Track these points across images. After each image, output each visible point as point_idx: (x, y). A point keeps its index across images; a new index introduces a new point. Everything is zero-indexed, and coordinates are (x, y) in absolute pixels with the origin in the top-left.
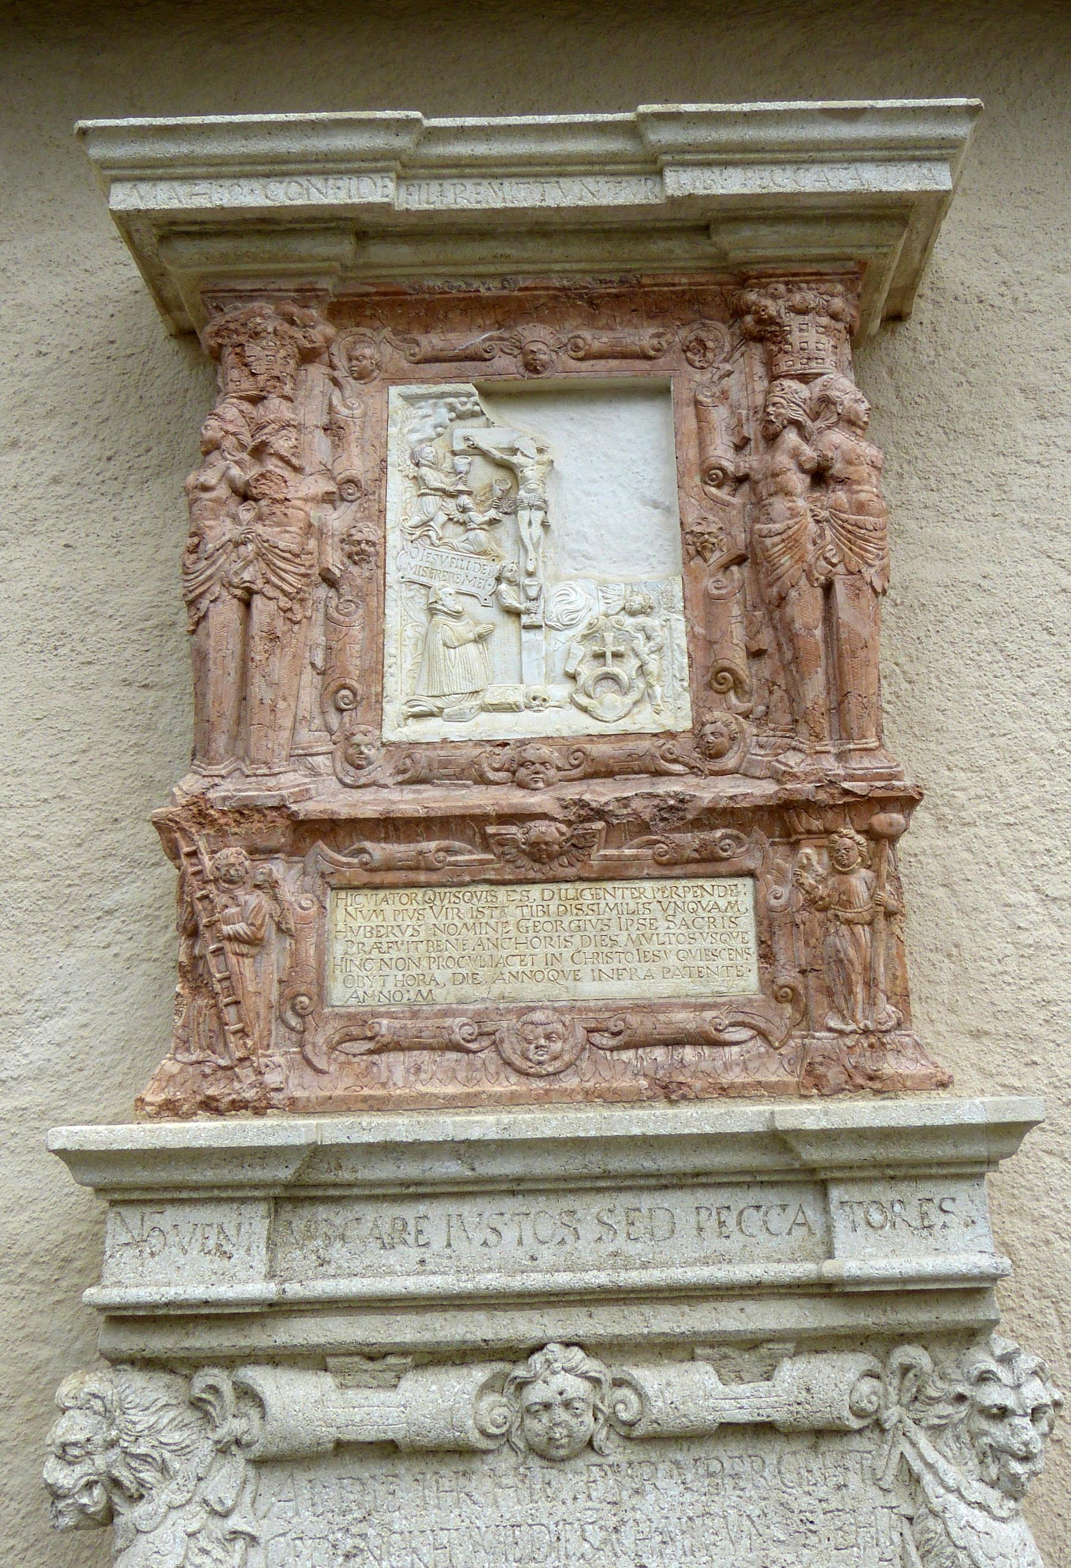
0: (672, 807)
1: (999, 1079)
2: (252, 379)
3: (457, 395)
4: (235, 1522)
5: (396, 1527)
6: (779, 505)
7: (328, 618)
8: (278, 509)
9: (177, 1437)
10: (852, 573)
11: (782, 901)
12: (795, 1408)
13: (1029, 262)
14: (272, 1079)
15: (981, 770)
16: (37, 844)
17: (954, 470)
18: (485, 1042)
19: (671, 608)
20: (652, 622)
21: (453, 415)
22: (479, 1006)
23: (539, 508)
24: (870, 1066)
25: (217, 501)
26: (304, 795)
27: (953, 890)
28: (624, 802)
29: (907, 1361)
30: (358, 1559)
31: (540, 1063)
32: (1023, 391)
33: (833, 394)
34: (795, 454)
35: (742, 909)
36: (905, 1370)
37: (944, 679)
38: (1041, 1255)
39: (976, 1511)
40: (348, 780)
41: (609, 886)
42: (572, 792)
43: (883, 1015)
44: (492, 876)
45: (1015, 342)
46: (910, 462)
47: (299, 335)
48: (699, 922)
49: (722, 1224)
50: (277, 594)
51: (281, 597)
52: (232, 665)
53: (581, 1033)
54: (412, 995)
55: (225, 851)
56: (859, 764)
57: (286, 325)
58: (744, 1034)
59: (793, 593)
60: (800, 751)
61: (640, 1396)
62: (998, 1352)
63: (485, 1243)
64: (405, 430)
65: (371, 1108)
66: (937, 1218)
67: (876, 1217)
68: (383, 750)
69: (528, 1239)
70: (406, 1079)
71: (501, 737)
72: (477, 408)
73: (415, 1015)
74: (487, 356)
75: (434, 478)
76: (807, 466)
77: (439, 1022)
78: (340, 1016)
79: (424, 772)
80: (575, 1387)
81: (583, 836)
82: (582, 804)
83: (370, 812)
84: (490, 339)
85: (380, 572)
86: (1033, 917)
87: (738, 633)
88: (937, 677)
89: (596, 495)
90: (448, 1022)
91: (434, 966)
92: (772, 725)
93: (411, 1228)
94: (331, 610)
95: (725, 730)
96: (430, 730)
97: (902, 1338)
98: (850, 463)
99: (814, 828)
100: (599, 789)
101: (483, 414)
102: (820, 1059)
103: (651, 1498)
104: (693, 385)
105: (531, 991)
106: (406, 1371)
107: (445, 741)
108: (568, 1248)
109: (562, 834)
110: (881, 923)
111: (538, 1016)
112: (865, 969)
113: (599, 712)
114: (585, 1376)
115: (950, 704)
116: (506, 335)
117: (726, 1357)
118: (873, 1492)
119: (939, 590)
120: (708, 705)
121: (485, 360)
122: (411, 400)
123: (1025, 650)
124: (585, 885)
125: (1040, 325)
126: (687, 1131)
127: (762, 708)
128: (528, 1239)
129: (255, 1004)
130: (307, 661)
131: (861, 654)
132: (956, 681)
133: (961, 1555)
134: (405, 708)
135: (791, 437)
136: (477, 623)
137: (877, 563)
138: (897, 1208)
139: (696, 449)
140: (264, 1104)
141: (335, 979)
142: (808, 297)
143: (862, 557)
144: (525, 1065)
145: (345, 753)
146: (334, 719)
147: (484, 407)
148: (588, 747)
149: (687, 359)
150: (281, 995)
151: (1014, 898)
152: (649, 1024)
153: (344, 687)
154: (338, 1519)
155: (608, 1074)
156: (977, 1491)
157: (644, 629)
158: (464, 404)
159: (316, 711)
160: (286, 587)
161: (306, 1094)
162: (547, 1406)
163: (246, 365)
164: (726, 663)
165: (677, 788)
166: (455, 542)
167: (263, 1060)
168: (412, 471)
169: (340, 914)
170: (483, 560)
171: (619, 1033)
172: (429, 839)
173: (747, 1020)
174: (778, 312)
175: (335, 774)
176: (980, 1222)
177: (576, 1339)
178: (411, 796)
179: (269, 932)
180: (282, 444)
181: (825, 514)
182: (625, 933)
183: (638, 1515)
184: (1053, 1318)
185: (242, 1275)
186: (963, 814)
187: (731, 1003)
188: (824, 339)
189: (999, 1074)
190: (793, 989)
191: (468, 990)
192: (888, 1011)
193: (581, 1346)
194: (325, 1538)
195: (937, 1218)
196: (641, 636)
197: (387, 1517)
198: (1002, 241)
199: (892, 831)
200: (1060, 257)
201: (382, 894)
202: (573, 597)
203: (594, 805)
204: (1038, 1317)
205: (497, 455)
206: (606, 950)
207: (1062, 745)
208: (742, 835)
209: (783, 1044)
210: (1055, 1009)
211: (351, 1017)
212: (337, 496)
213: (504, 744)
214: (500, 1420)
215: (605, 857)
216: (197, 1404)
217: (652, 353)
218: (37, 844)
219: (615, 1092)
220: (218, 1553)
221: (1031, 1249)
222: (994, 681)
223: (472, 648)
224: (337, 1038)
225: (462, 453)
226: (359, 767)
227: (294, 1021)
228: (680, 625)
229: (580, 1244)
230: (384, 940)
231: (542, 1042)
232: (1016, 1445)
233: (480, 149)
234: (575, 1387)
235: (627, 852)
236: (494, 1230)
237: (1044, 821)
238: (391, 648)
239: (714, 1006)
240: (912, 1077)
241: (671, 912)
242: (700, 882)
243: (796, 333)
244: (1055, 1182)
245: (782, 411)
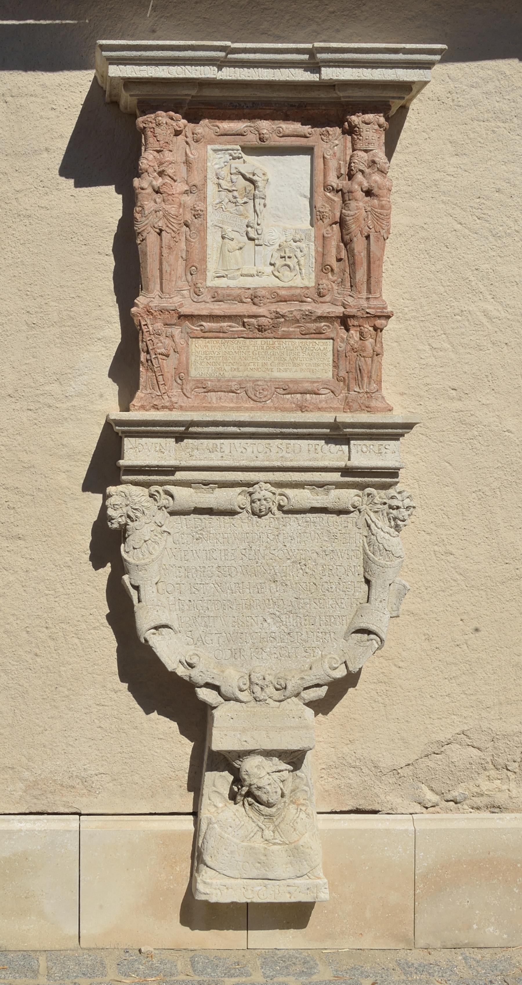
0: (306, 315)
1: (408, 409)
2: (157, 142)
3: (233, 150)
4: (164, 528)
5: (211, 532)
6: (353, 204)
7: (186, 239)
8: (170, 198)
9: (146, 504)
10: (376, 232)
11: (342, 349)
12: (334, 503)
13: (461, 83)
14: (174, 399)
15: (415, 300)
16: (72, 314)
17: (419, 178)
18: (242, 390)
19: (310, 240)
20: (302, 245)
21: (231, 157)
22: (240, 379)
23: (263, 199)
24: (367, 403)
25: (148, 194)
26: (181, 305)
27: (400, 344)
28: (291, 312)
29: (369, 492)
30: (200, 540)
31: (260, 398)
32: (451, 142)
33: (377, 159)
34: (360, 184)
35: (328, 350)
36: (369, 495)
37: (405, 264)
38: (415, 467)
39: (386, 534)
40: (195, 300)
41: (284, 340)
42: (273, 307)
43: (372, 388)
44: (245, 336)
45: (451, 120)
46: (402, 173)
47: (174, 124)
48: (314, 354)
49: (316, 449)
50: (171, 231)
51: (173, 233)
52: (157, 258)
53: (273, 389)
54: (218, 374)
55: (157, 324)
56: (373, 303)
57: (170, 120)
58: (327, 391)
59: (355, 239)
60: (352, 297)
61: (287, 498)
62: (398, 491)
63: (242, 452)
64: (213, 164)
65: (206, 410)
66: (384, 451)
67: (365, 449)
68: (207, 289)
69: (255, 451)
70: (217, 402)
71: (248, 286)
72: (240, 155)
73: (219, 381)
74: (245, 134)
75: (225, 184)
76: (364, 189)
77: (227, 383)
78: (194, 380)
79: (221, 298)
80: (269, 495)
81: (276, 323)
82: (277, 313)
83: (205, 312)
84: (246, 126)
85: (205, 222)
86: (427, 355)
87: (334, 251)
88: (403, 263)
89: (283, 192)
90: (230, 384)
91: (225, 365)
92: (343, 286)
93: (219, 447)
94: (188, 237)
95: (326, 287)
96: (223, 283)
97: (368, 486)
98: (380, 189)
99: (355, 325)
100: (282, 307)
101: (242, 157)
102: (350, 401)
103: (288, 527)
104: (323, 149)
105: (257, 375)
106: (215, 489)
107: (228, 287)
108: (267, 454)
109: (270, 323)
110: (375, 357)
111: (259, 383)
112: (368, 372)
113: (282, 278)
114: (270, 492)
115: (406, 274)
116: (252, 125)
117: (314, 489)
118: (355, 528)
119: (407, 228)
120: (321, 277)
121: (244, 136)
122: (215, 151)
123: (437, 254)
124: (276, 340)
125: (462, 112)
126: (308, 421)
127: (340, 280)
128: (255, 451)
129: (168, 375)
130: (180, 256)
131: (377, 263)
132: (409, 265)
133: (380, 545)
134: (214, 274)
135: (359, 176)
136: (239, 243)
137: (386, 228)
138: (371, 447)
139: (323, 177)
140: (172, 407)
141: (192, 368)
142: (370, 117)
143: (381, 226)
144: (255, 398)
145: (194, 290)
146: (189, 277)
147: (243, 155)
148: (278, 291)
149: (322, 138)
150: (175, 373)
151: (420, 347)
152: (296, 387)
153: (193, 266)
154: (194, 529)
155: (282, 402)
156: (387, 529)
157: (300, 248)
158: (235, 153)
159: (183, 274)
160: (174, 229)
161: (185, 405)
162: (259, 500)
163: (155, 137)
164: (329, 263)
165: (309, 308)
166: (231, 210)
167: (171, 394)
168: (216, 181)
169: (193, 346)
170: (242, 218)
171: (286, 390)
172: (224, 322)
173: (328, 387)
174: (359, 122)
175: (190, 297)
176: (397, 452)
177: (268, 481)
178: (217, 307)
179: (172, 352)
180: (170, 171)
181: (369, 209)
182: (289, 357)
183: (284, 532)
184: (416, 486)
185: (168, 458)
186: (406, 316)
187: (323, 381)
188: (375, 135)
189: (408, 408)
190: (344, 378)
191: (236, 373)
192: (374, 386)
193: (270, 483)
194: (190, 534)
195: (384, 451)
196: (298, 250)
197: (209, 529)
198: (451, 72)
199: (381, 327)
200: (475, 80)
201: (207, 340)
202: (274, 234)
203: (281, 313)
204: (412, 485)
205: (248, 176)
206: (282, 362)
207: (446, 292)
208: (330, 325)
209: (339, 395)
210: (430, 387)
211: (198, 381)
212: (189, 192)
213: (249, 289)
214: (244, 503)
215: (284, 331)
216: (151, 496)
217: (308, 135)
218: (72, 314)
219: (284, 408)
220: (160, 536)
221: (412, 465)
222: (424, 266)
223: (237, 252)
224: (193, 387)
225: (235, 174)
226: (199, 295)
227: (179, 381)
228: (313, 247)
229: (271, 454)
230: (208, 356)
231: (261, 391)
232: (400, 517)
233: (251, 56)
234: (269, 495)
235: (291, 329)
236: (245, 448)
237: (435, 320)
238: (209, 251)
239: (317, 382)
240: (380, 408)
241: (304, 350)
242: (315, 340)
243: (365, 132)
244: (423, 444)
245: (357, 165)
